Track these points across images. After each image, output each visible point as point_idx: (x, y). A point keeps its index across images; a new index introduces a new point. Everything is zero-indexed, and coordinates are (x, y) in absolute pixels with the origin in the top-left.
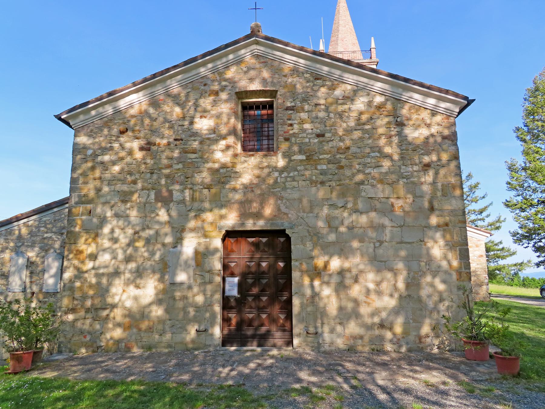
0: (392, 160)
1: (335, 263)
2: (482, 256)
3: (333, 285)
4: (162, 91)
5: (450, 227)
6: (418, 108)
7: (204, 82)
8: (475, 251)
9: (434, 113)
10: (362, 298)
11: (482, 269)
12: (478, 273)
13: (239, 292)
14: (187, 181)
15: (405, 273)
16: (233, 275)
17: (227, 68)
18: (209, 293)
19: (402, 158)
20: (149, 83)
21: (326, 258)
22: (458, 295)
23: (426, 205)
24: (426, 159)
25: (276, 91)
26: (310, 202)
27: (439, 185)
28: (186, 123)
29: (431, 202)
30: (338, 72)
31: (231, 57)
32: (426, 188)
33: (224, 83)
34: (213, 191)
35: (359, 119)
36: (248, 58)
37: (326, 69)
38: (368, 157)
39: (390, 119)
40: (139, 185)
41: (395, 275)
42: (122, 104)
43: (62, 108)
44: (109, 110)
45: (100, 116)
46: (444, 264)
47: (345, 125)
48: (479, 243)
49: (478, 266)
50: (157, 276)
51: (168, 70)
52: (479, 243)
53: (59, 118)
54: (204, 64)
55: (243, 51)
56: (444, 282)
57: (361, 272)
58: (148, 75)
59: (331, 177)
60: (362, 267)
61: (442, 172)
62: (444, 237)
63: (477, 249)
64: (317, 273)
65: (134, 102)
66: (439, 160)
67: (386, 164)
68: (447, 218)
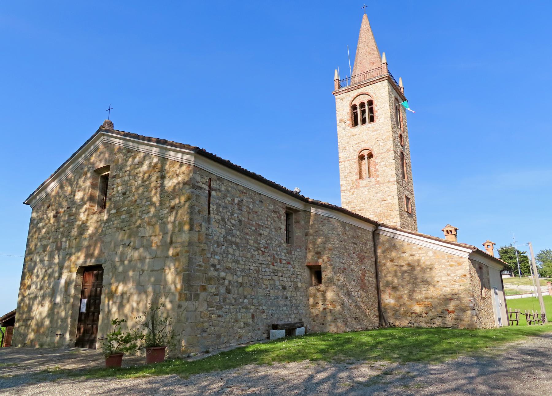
0: (155, 207)
1: (121, 288)
2: (465, 275)
3: (117, 304)
4: (64, 178)
5: (179, 256)
6: (173, 163)
7: (81, 166)
8: (457, 270)
9: (181, 165)
10: (129, 314)
11: (466, 290)
12: (462, 295)
13: (86, 310)
14: (67, 235)
15: (152, 294)
16: (85, 298)
17: (92, 155)
18: (67, 310)
19: (161, 204)
20: (58, 174)
21: (117, 284)
22: (177, 312)
23: (169, 240)
24: (173, 203)
25: (109, 166)
26: (115, 243)
27: (177, 222)
28: (72, 196)
29: (171, 238)
30: (136, 145)
31: (92, 147)
32: (170, 226)
33: (90, 166)
34: (77, 240)
35: (143, 179)
36: (101, 147)
37: (131, 144)
38: (144, 206)
39: (159, 174)
40: (51, 241)
41: (147, 296)
42: (49, 189)
43: (25, 199)
44: (43, 195)
45: (41, 199)
46: (173, 287)
47: (136, 183)
48: (461, 260)
49: (462, 288)
50: (50, 299)
51: (64, 164)
52: (461, 260)
53: (24, 203)
54: (80, 156)
55: (97, 142)
56: (171, 302)
57: (131, 294)
58: (56, 170)
59: (125, 223)
60: (132, 290)
61: (180, 212)
62: (174, 265)
63: (459, 267)
64: (111, 295)
65: (53, 186)
66: (180, 202)
67: (152, 210)
68: (179, 249)
